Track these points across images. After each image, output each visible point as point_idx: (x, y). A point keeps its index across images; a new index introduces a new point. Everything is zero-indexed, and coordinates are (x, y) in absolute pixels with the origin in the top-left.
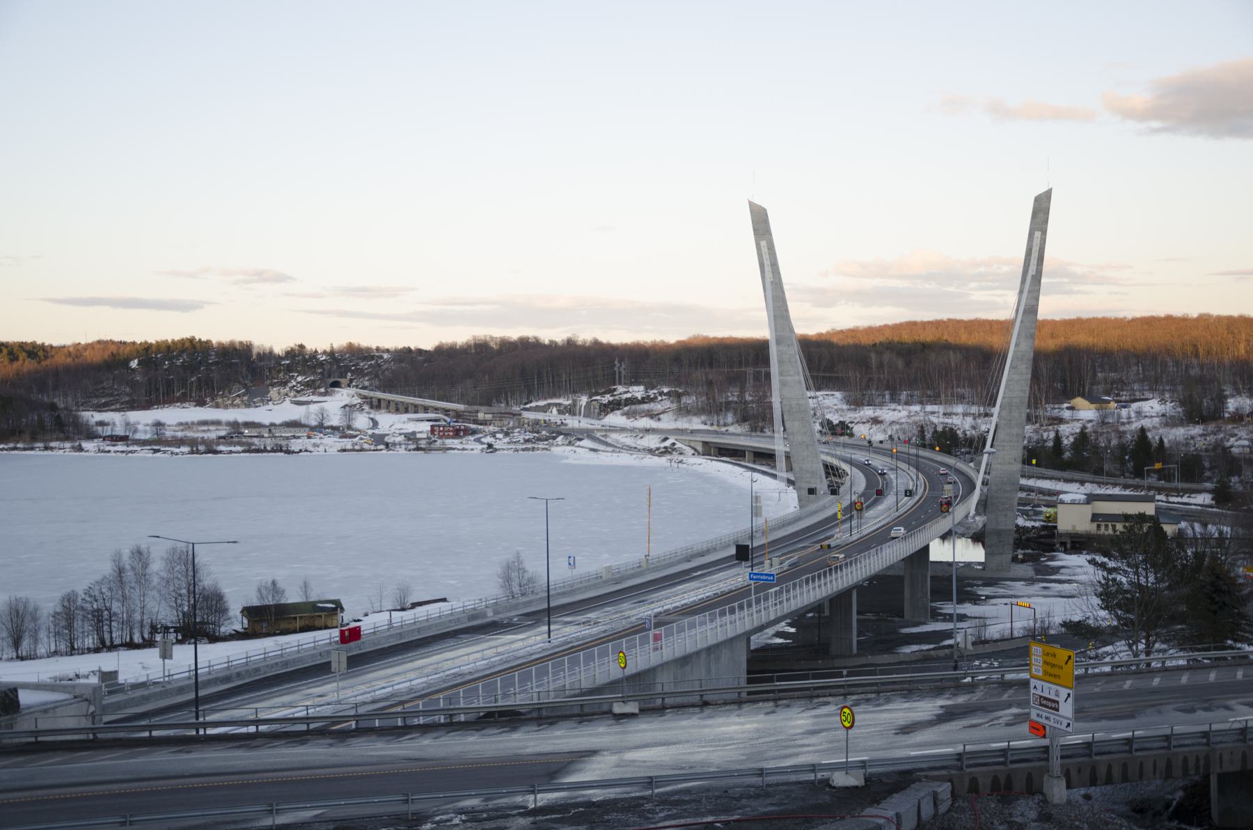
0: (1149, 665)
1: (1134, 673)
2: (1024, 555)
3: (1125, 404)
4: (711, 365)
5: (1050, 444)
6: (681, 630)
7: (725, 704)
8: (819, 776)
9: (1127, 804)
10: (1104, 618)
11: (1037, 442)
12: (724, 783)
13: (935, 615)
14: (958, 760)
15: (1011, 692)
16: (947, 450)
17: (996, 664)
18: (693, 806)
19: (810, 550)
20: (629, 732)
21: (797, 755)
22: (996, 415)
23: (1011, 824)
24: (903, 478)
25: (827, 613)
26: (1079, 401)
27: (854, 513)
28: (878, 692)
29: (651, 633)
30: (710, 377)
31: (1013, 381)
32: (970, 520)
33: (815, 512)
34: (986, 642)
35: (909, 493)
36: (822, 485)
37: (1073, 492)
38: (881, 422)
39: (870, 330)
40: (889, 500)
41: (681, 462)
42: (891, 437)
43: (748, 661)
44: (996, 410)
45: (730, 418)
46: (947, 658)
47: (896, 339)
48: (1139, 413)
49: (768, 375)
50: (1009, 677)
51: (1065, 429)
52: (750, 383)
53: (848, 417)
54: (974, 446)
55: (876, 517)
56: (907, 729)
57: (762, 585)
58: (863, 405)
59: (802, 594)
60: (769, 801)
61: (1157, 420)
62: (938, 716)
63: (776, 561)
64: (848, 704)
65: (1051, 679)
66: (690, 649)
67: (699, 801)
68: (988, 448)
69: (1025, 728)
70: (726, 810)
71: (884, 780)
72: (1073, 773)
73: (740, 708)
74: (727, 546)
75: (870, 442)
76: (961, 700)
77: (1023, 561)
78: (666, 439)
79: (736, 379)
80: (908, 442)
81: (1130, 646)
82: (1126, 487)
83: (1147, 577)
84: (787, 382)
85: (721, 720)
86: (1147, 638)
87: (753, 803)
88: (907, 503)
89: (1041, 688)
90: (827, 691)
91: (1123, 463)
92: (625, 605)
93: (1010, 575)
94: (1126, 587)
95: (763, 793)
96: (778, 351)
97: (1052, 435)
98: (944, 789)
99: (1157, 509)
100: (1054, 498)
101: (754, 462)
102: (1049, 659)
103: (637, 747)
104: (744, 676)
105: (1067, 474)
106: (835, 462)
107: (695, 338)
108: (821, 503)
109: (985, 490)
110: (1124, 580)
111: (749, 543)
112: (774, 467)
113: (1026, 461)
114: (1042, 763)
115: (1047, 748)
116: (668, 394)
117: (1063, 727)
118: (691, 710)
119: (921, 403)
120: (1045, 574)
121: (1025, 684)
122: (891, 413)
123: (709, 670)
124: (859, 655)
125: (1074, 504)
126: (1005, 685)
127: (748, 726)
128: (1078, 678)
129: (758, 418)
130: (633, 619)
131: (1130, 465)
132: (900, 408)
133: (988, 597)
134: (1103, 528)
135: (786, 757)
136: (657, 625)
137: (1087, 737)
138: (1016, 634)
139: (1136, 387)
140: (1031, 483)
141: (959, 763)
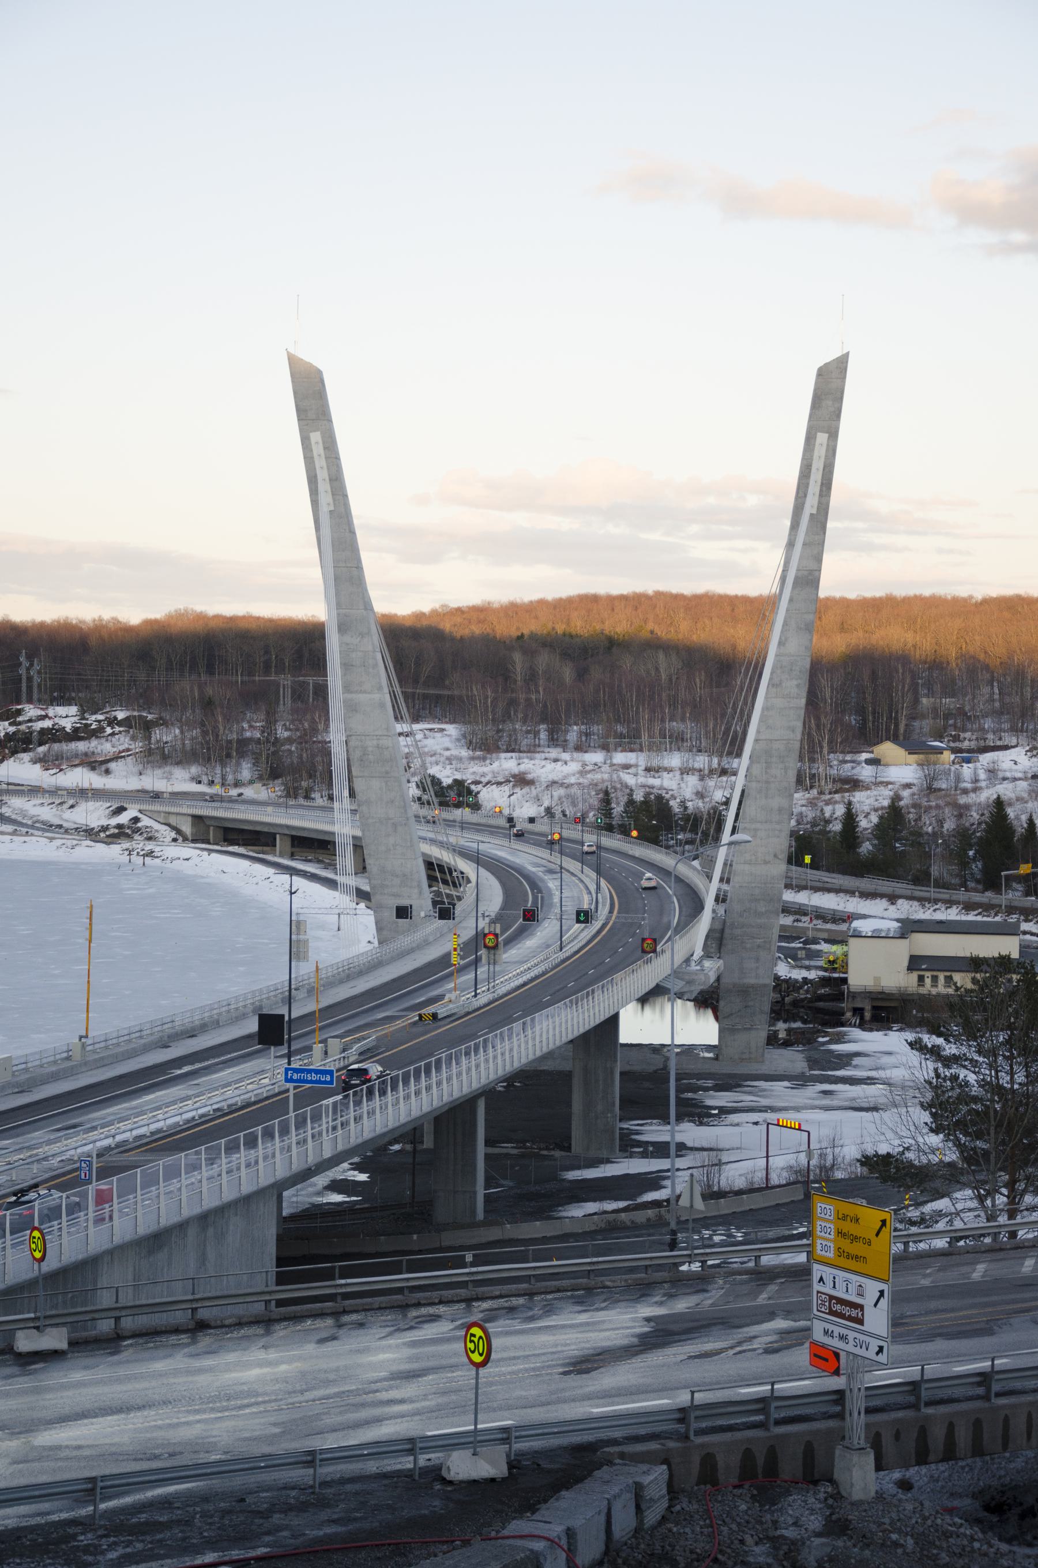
0: (1013, 1235)
1: (990, 1250)
2: (789, 1031)
3: (967, 756)
4: (210, 670)
5: (837, 827)
6: (151, 1181)
7: (240, 1324)
8: (422, 1460)
9: (974, 1496)
10: (936, 1148)
11: (814, 824)
12: (237, 1482)
13: (628, 1145)
14: (681, 1421)
15: (773, 1288)
16: (651, 837)
17: (739, 1236)
18: (177, 1532)
19: (399, 1024)
20: (49, 1389)
21: (378, 1420)
22: (742, 773)
23: (775, 1542)
24: (572, 888)
25: (428, 1143)
26: (888, 749)
27: (483, 952)
28: (531, 1294)
29: (91, 1189)
30: (209, 691)
31: (774, 712)
32: (694, 967)
33: (410, 951)
34: (721, 1194)
35: (584, 917)
36: (422, 901)
37: (877, 915)
38: (531, 783)
39: (513, 610)
40: (546, 930)
41: (150, 854)
42: (549, 811)
43: (280, 1239)
44: (743, 764)
45: (246, 771)
46: (652, 1225)
47: (560, 628)
48: (992, 772)
49: (322, 692)
50: (767, 1260)
51: (863, 800)
52: (286, 704)
53: (471, 772)
54: (701, 829)
55: (525, 959)
56: (584, 1365)
57: (309, 1092)
58: (497, 749)
59: (383, 1108)
60: (324, 1515)
61: (1023, 785)
62: (642, 1336)
63: (334, 1045)
64: (476, 1317)
65: (852, 1264)
66: (168, 1218)
67: (188, 1523)
68: (726, 837)
69: (802, 1356)
70: (242, 1539)
71: (545, 1465)
72: (887, 1440)
73: (268, 1332)
74: (240, 1017)
75: (510, 820)
76: (682, 1305)
77: (786, 1044)
78: (120, 810)
79: (261, 698)
80: (580, 820)
81: (981, 1199)
82: (968, 907)
83: (1012, 1074)
84: (358, 702)
85: (231, 1357)
86: (1011, 1185)
87: (295, 1520)
88: (580, 935)
89: (831, 1281)
90: (435, 1295)
91: (964, 863)
92: (38, 1135)
93: (764, 1069)
94: (975, 1091)
95: (313, 1499)
96: (341, 644)
97: (840, 810)
98: (654, 1478)
99: (1024, 948)
100: (843, 927)
101: (292, 856)
102: (848, 1227)
103: (64, 1419)
104: (271, 1267)
105: (866, 883)
106: (446, 857)
107: (180, 615)
108: (418, 936)
109: (721, 911)
110: (972, 1078)
111: (284, 1011)
112: (331, 866)
113: (795, 859)
114: (831, 1423)
115: (840, 1393)
116: (127, 723)
117: (871, 1354)
118: (173, 1339)
119: (605, 747)
120: (826, 1067)
121: (801, 1274)
122: (550, 766)
123: (203, 1259)
124: (487, 1223)
125: (879, 939)
126: (763, 1276)
127: (284, 1367)
128: (898, 1259)
129: (303, 771)
130: (54, 1162)
131: (977, 867)
132: (566, 756)
133: (724, 1111)
134: (928, 981)
135: (367, 1423)
136: (105, 1173)
137: (913, 1372)
138: (775, 1180)
139: (988, 723)
140: (802, 898)
141: (681, 1428)
